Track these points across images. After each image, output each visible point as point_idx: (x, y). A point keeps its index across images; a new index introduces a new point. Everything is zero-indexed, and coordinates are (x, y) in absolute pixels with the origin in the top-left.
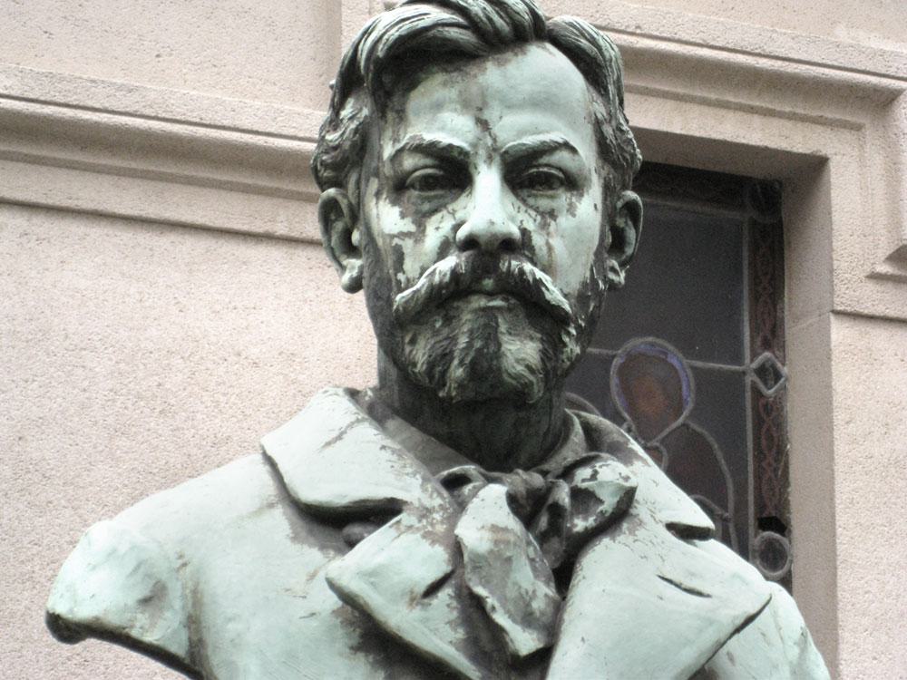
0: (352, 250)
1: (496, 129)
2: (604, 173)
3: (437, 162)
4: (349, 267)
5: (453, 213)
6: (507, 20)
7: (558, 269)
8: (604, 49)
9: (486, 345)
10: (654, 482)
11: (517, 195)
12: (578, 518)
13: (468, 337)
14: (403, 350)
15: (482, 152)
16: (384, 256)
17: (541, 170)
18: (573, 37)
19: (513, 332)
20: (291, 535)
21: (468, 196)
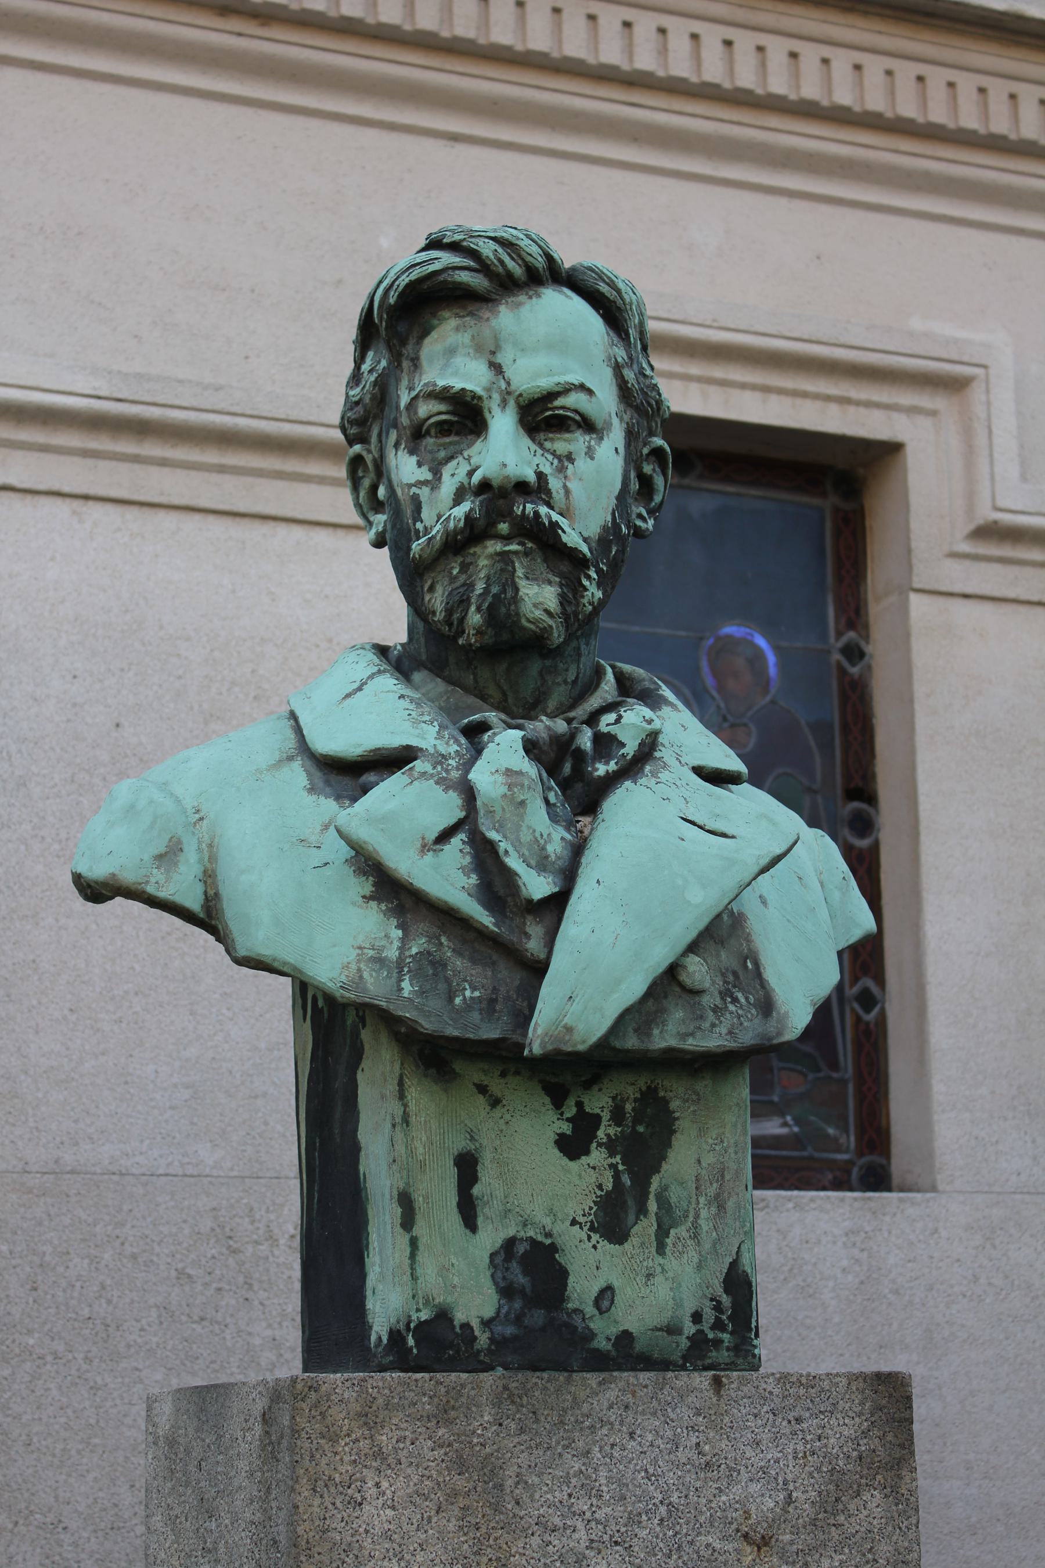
0: (378, 506)
1: (509, 373)
2: (627, 418)
3: (450, 408)
4: (376, 522)
5: (468, 459)
6: (520, 262)
7: (577, 512)
8: (623, 291)
10: (683, 726)
11: (533, 440)
12: (600, 762)
13: (485, 583)
14: (423, 599)
15: (496, 397)
16: (403, 507)
17: (556, 412)
18: (590, 279)
19: (530, 576)
20: (308, 786)
21: (483, 441)
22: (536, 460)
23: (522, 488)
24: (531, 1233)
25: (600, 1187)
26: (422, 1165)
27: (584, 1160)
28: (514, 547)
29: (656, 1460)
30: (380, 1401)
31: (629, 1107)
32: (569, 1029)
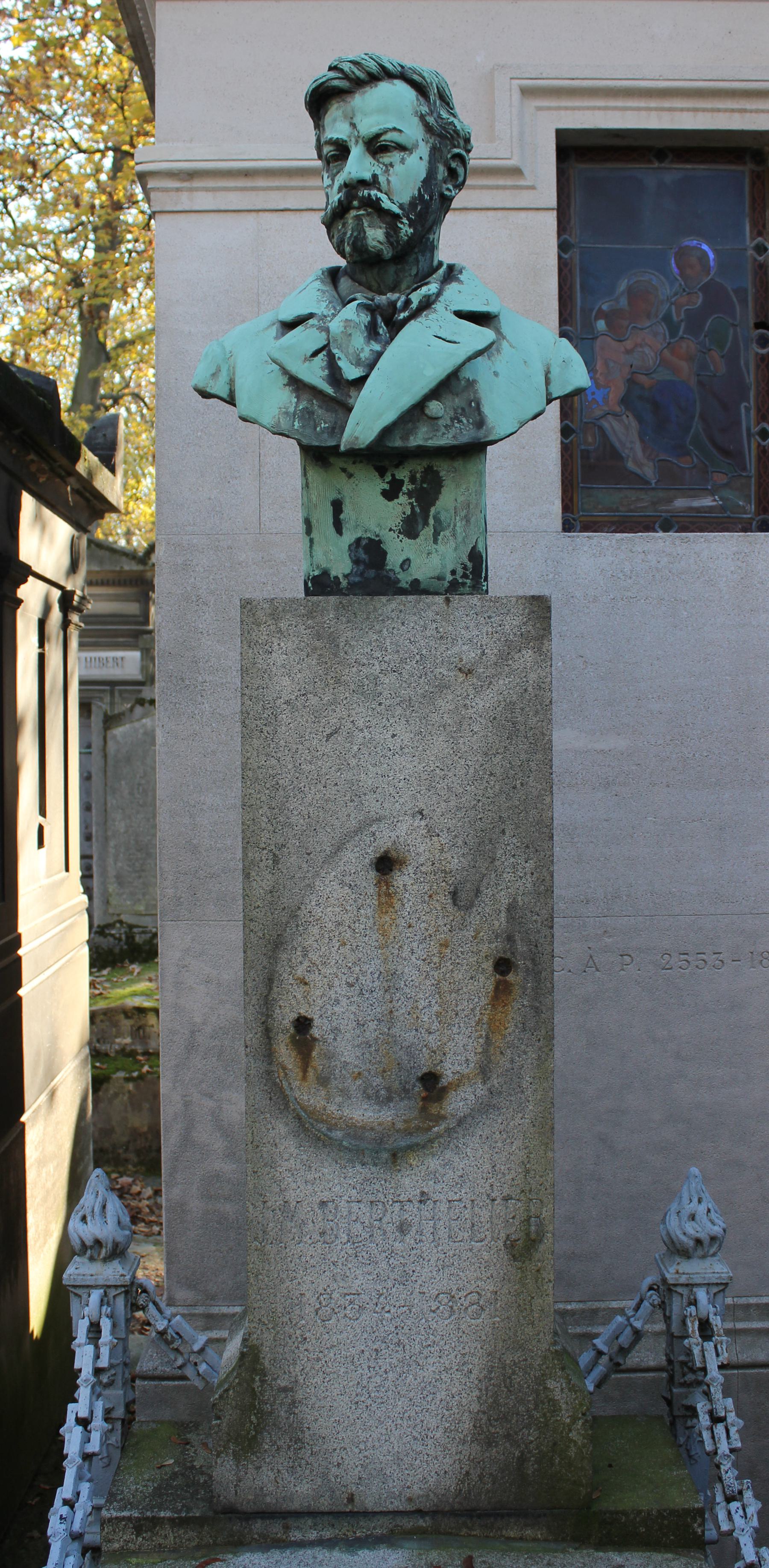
1: (359, 127)
9: (359, 234)
11: (374, 158)
15: (353, 140)
22: (373, 168)
23: (363, 183)
24: (369, 535)
25: (404, 513)
26: (316, 506)
27: (396, 501)
28: (362, 212)
29: (415, 635)
30: (280, 609)
31: (418, 476)
32: (357, 438)
